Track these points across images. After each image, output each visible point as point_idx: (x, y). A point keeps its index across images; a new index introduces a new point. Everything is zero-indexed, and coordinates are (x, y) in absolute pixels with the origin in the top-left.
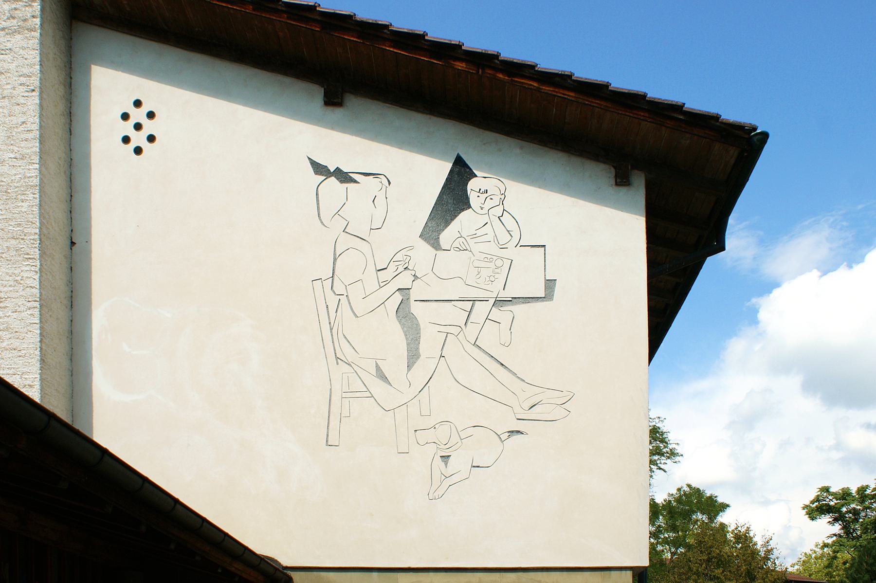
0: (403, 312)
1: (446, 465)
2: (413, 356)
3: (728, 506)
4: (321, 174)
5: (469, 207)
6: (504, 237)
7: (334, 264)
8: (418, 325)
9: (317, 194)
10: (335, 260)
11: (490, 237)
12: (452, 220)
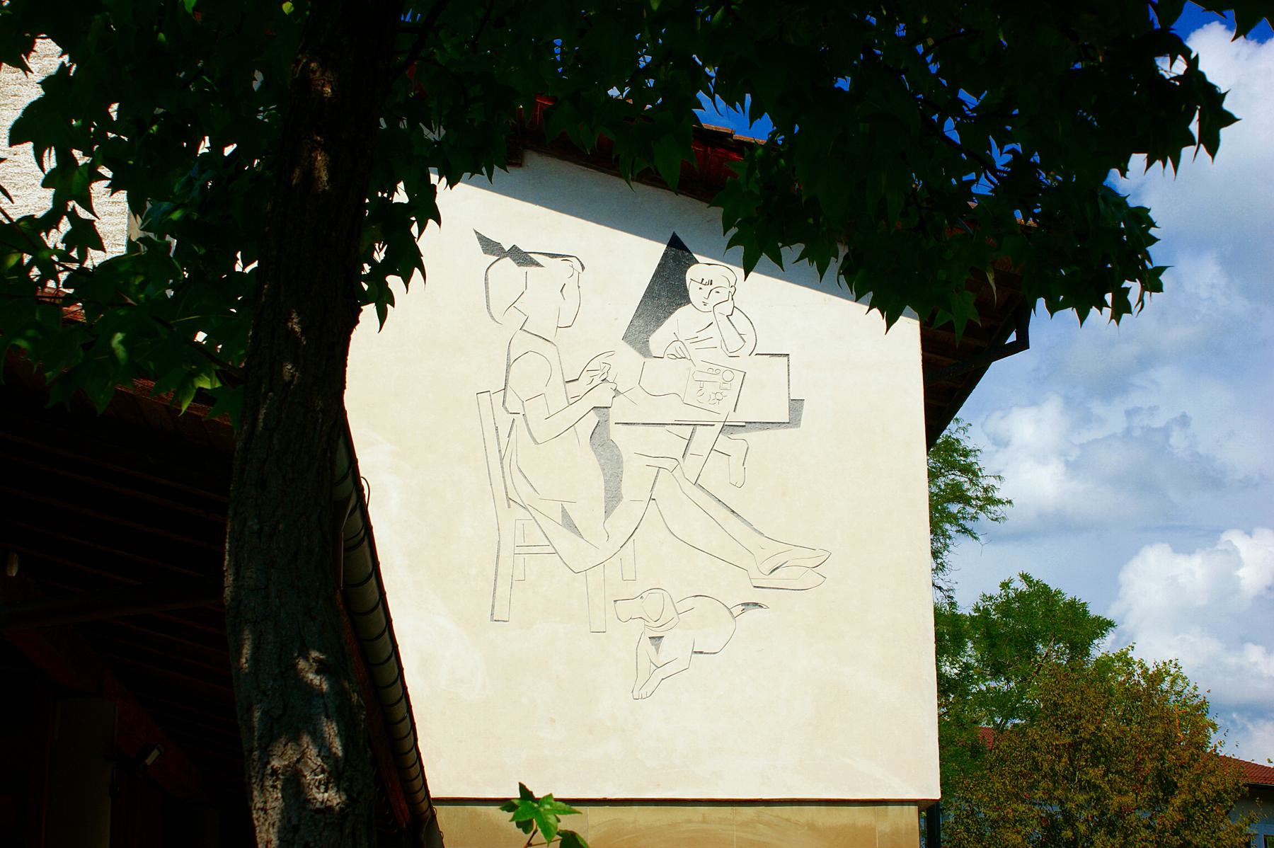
0: (600, 438)
1: (657, 650)
2: (613, 498)
3: (1110, 624)
4: (492, 253)
5: (689, 302)
6: (734, 343)
7: (507, 372)
8: (619, 456)
9: (486, 279)
10: (509, 366)
11: (716, 341)
12: (666, 318)
